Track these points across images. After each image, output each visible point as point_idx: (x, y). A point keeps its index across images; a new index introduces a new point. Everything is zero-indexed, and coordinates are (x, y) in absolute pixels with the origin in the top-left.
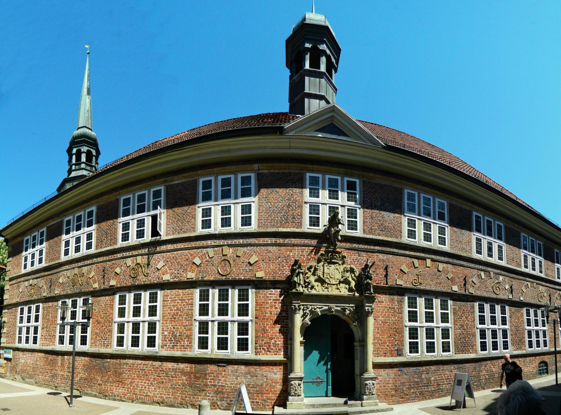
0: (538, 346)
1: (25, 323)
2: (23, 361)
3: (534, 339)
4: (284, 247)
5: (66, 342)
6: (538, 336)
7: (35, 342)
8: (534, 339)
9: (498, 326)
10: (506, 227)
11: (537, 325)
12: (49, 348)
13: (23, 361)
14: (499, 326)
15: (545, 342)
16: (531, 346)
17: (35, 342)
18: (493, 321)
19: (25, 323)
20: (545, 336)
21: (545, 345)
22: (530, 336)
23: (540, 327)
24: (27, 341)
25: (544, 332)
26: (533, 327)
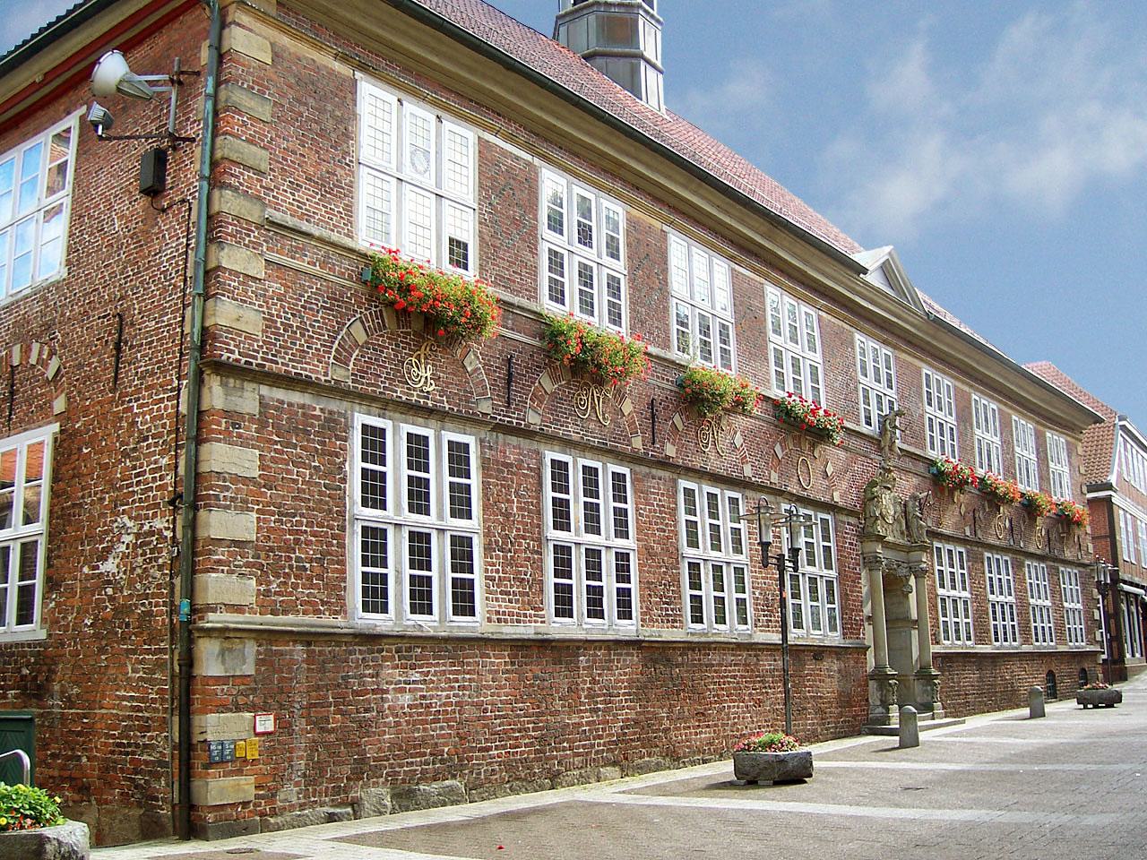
0: (595, 609)
1: (396, 511)
2: (406, 699)
3: (579, 582)
4: (357, 247)
5: (13, 576)
6: (594, 571)
7: (463, 601)
8: (579, 582)
9: (606, 539)
10: (999, 409)
11: (593, 524)
12: (526, 631)
13: (406, 699)
14: (577, 534)
15: (624, 597)
16: (564, 606)
17: (463, 601)
18: (419, 498)
19: (396, 511)
20: (623, 573)
21: (625, 613)
22: (563, 567)
23: (726, 555)
24: (421, 599)
25: (622, 557)
26: (705, 551)
